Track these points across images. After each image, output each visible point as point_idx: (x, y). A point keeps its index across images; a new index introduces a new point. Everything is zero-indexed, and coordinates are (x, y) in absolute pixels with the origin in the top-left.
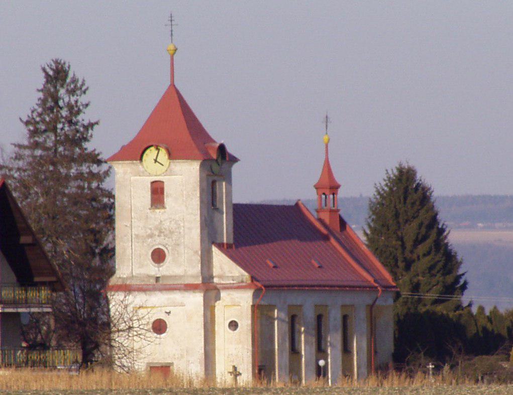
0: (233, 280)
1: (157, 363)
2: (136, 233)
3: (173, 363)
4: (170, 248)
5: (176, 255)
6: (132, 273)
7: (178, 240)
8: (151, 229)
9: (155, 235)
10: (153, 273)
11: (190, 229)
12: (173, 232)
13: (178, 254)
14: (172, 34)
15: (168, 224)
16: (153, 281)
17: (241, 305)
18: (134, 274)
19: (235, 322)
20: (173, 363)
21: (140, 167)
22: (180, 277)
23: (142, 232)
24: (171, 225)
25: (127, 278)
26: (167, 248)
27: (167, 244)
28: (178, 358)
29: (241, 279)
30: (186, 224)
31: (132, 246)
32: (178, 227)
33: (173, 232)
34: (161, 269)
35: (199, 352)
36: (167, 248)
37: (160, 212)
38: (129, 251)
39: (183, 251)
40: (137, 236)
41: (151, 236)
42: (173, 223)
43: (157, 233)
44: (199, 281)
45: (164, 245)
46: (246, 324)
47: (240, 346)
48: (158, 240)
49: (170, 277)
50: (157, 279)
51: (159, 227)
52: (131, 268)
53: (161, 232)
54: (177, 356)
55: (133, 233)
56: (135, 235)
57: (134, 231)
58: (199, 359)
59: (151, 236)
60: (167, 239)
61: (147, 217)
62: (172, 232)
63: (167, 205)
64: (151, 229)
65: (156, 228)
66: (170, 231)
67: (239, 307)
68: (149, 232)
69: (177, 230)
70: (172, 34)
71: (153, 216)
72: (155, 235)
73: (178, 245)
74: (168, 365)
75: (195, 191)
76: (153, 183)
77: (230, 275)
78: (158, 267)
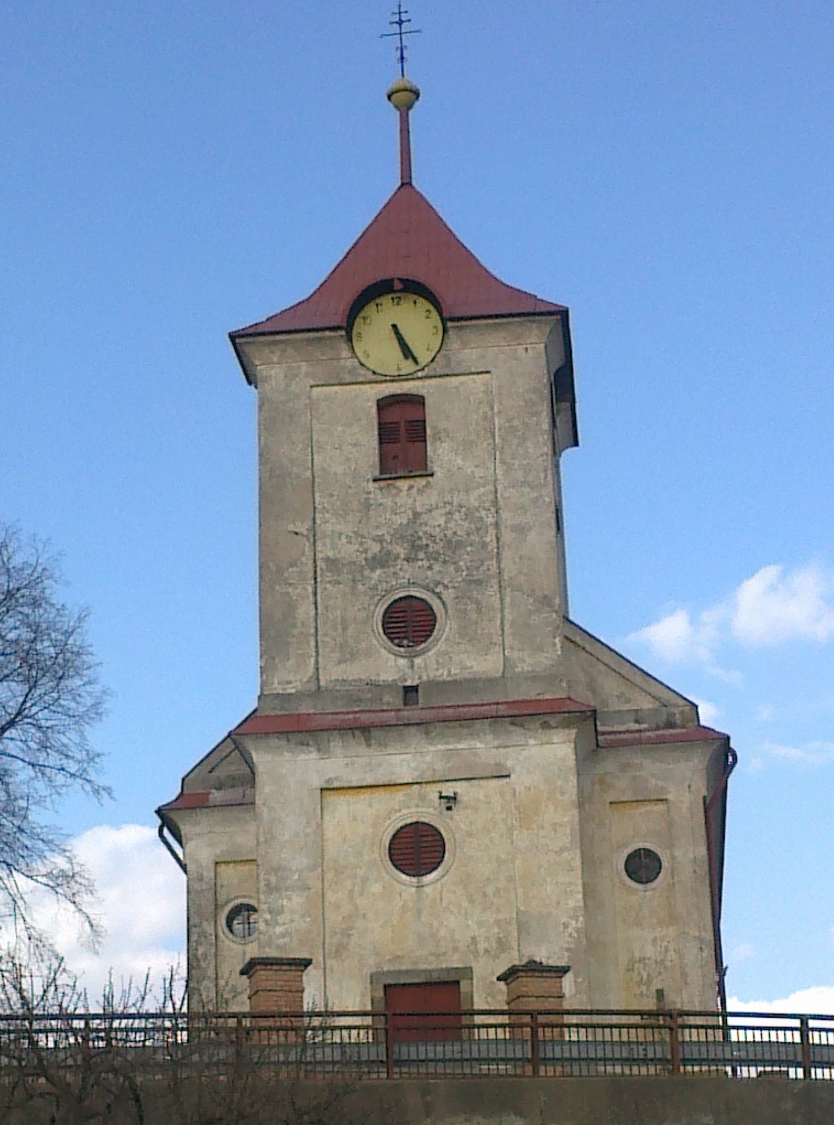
0: (637, 721)
1: (408, 972)
2: (330, 554)
3: (467, 972)
4: (448, 595)
5: (474, 616)
6: (318, 679)
7: (477, 568)
8: (380, 540)
9: (397, 557)
10: (388, 676)
11: (520, 530)
12: (459, 545)
13: (479, 611)
14: (402, 58)
15: (442, 521)
16: (394, 700)
17: (670, 797)
18: (322, 683)
19: (648, 852)
20: (467, 972)
21: (345, 353)
22: (491, 682)
23: (348, 551)
24: (452, 525)
25: (299, 696)
26: (439, 596)
27: (438, 583)
28: (487, 951)
29: (664, 718)
30: (505, 514)
31: (315, 594)
32: (478, 530)
33: (459, 545)
34: (418, 661)
35: (566, 926)
36: (439, 596)
37: (411, 487)
38: (305, 611)
39: (496, 601)
40: (333, 564)
41: (382, 561)
42: (457, 516)
43: (401, 550)
44: (329, 1009)
45: (427, 588)
46: (691, 856)
47: (671, 931)
48: (408, 572)
49: (455, 685)
50: (410, 691)
51: (410, 532)
52: (313, 660)
53: (415, 548)
54: (482, 946)
55: (319, 556)
56: (327, 560)
57: (325, 551)
58: (568, 950)
59: (382, 561)
60: (437, 567)
61: (367, 506)
62: (454, 545)
63: (435, 467)
64: (380, 540)
65: (399, 535)
66: (449, 542)
67: (661, 807)
68: (376, 548)
69: (475, 538)
70: (402, 58)
71: (388, 501)
72: (397, 557)
73: (479, 582)
74: (452, 977)
75: (536, 414)
76: (384, 404)
77: (626, 707)
78: (411, 657)
